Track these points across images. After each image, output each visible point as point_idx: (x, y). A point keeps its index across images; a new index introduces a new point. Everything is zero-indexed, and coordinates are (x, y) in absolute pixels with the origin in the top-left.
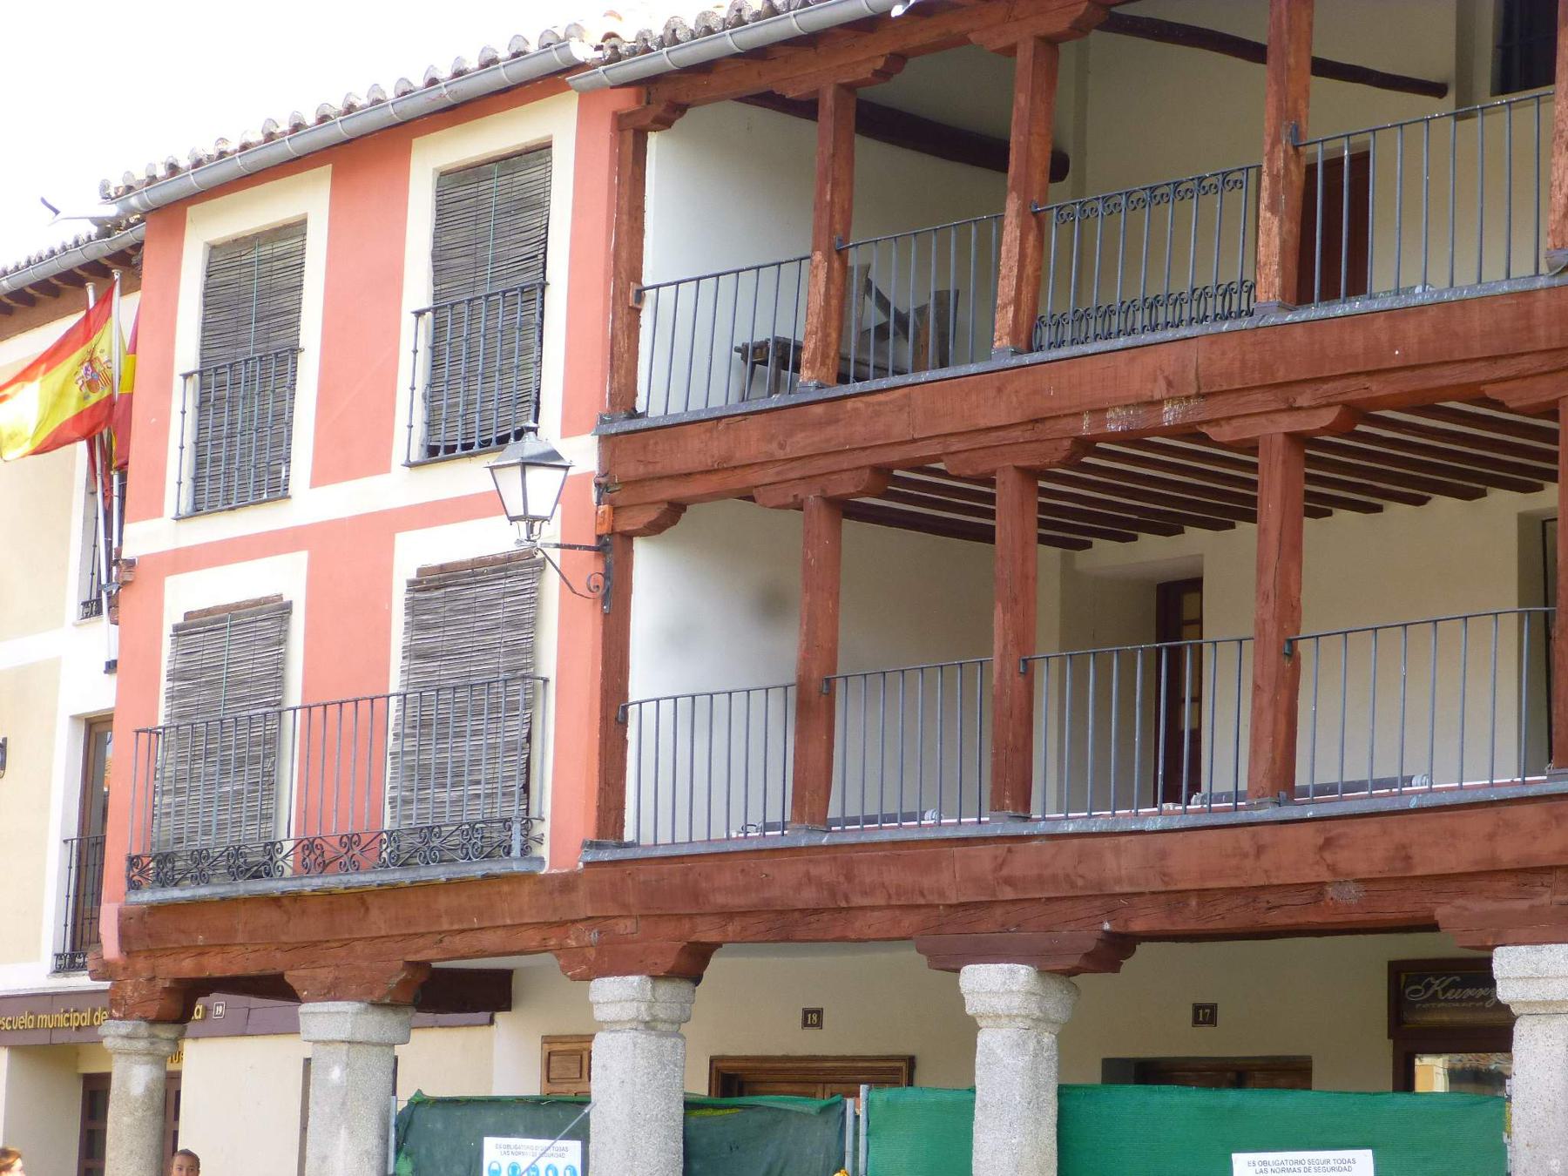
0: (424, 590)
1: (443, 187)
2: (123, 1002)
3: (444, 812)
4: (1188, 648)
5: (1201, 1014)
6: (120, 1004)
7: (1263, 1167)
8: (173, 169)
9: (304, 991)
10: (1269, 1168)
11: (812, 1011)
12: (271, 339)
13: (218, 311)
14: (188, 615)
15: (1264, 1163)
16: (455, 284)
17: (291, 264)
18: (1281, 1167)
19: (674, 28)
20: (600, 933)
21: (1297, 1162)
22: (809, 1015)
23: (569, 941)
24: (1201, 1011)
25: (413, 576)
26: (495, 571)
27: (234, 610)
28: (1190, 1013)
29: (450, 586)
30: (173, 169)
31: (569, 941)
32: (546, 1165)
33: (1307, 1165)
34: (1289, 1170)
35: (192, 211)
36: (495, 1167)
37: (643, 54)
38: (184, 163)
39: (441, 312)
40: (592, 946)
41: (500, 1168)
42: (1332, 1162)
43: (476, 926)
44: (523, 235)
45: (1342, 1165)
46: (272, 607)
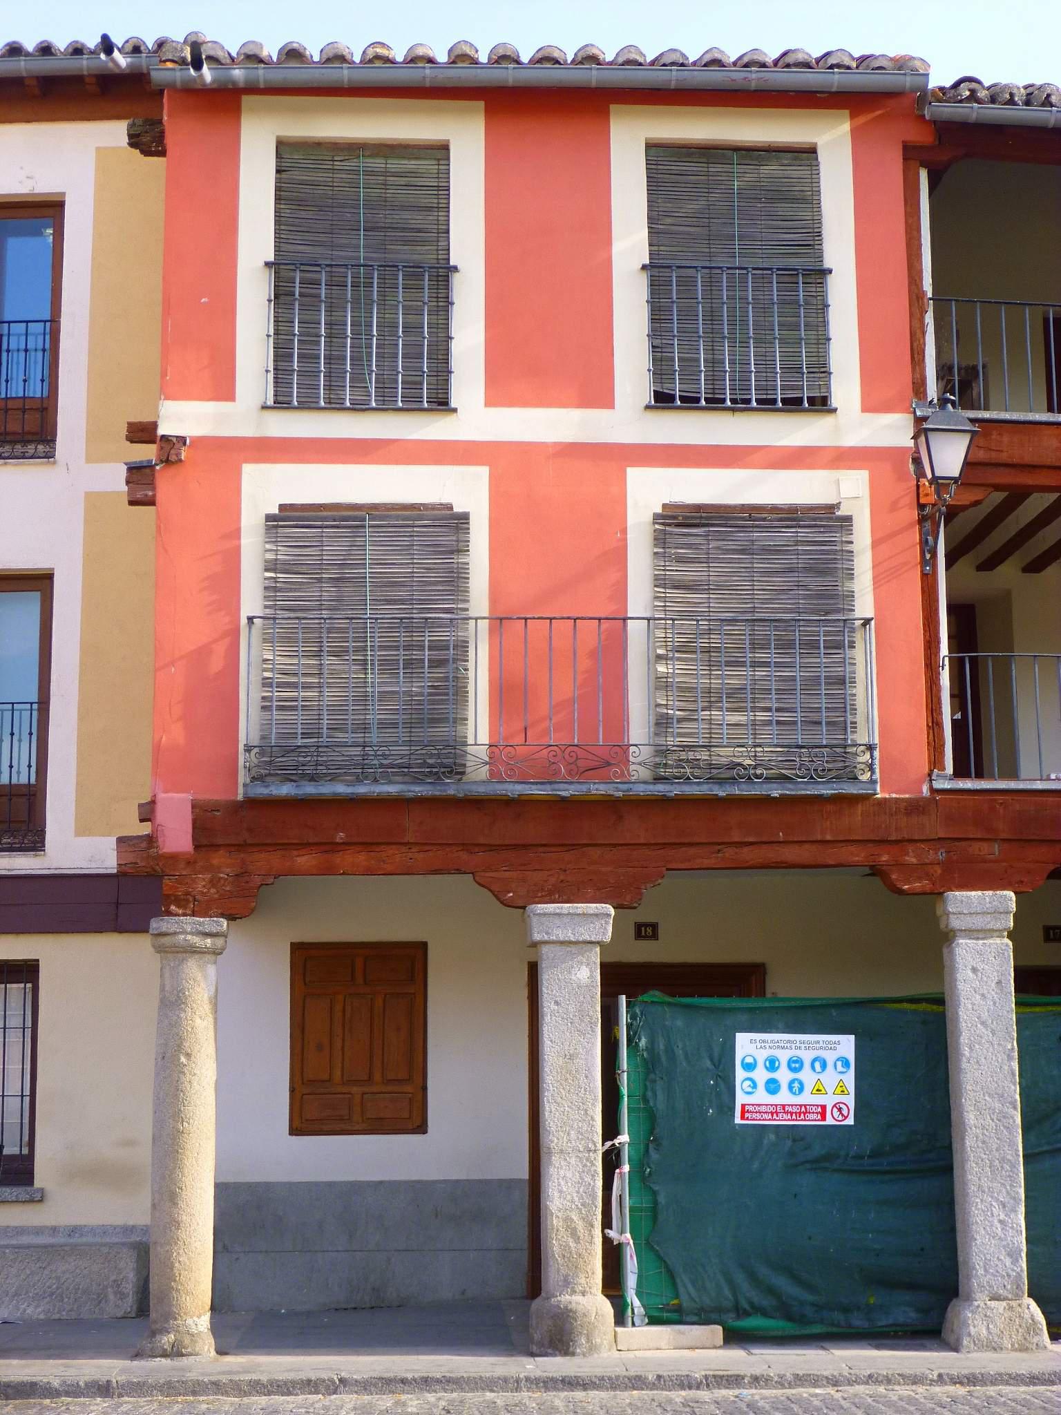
0: (678, 525)
1: (657, 157)
2: (191, 899)
3: (347, 724)
4: (990, 659)
5: (1052, 934)
6: (188, 901)
7: (763, 1045)
8: (107, 45)
9: (509, 892)
10: (767, 1045)
11: (646, 925)
12: (387, 251)
13: (298, 207)
14: (282, 507)
15: (764, 1041)
16: (680, 249)
17: (416, 184)
18: (776, 1045)
19: (1049, 92)
20: (948, 852)
21: (789, 1041)
22: (1051, 932)
23: (907, 858)
24: (1051, 932)
25: (659, 510)
26: (781, 520)
27: (373, 509)
28: (1041, 933)
29: (713, 525)
30: (107, 45)
31: (907, 858)
32: (813, 1057)
33: (798, 1044)
34: (783, 1048)
35: (246, 100)
36: (749, 1060)
37: (1005, 104)
38: (118, 40)
39: (656, 270)
40: (939, 864)
41: (755, 1060)
42: (821, 1043)
43: (781, 840)
44: (782, 222)
45: (830, 1046)
46: (447, 514)
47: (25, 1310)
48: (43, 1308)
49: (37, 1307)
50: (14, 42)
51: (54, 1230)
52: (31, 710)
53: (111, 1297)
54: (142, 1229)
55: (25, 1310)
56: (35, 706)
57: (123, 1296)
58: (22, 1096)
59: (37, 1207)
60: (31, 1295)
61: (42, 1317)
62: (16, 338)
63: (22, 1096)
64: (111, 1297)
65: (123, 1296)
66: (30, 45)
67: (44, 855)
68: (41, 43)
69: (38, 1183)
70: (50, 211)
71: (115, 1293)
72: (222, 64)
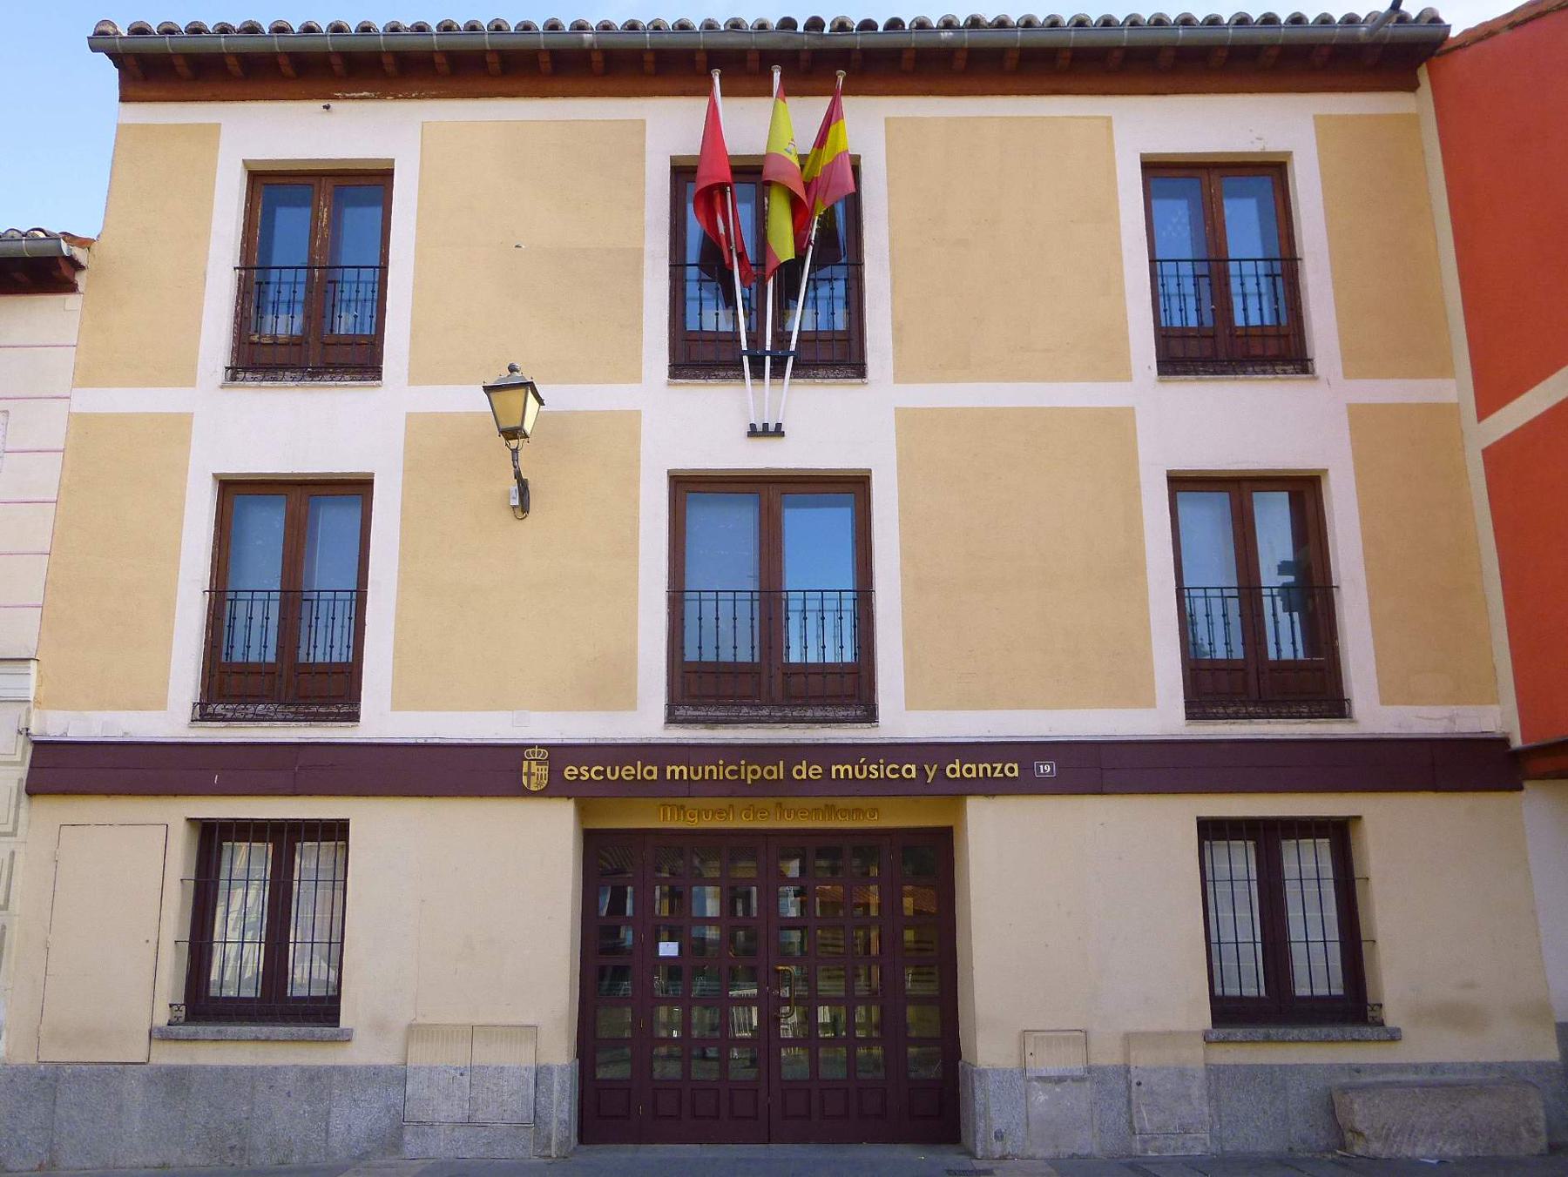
22: (1042, 767)
24: (1042, 767)
47: (1441, 1149)
48: (1458, 1145)
49: (1452, 1145)
50: (1270, 13)
51: (1417, 1068)
52: (752, 600)
53: (1525, 1135)
54: (1500, 1067)
55: (1441, 1149)
56: (756, 595)
57: (1534, 1133)
58: (1219, 943)
59: (1393, 1045)
60: (1445, 1133)
61: (1459, 1154)
62: (348, 285)
63: (1255, 942)
64: (1525, 1135)
65: (1534, 1133)
66: (1255, 16)
67: (878, 726)
68: (1294, 14)
69: (344, 1021)
70: (377, 180)
71: (1528, 1132)
72: (1139, 25)
